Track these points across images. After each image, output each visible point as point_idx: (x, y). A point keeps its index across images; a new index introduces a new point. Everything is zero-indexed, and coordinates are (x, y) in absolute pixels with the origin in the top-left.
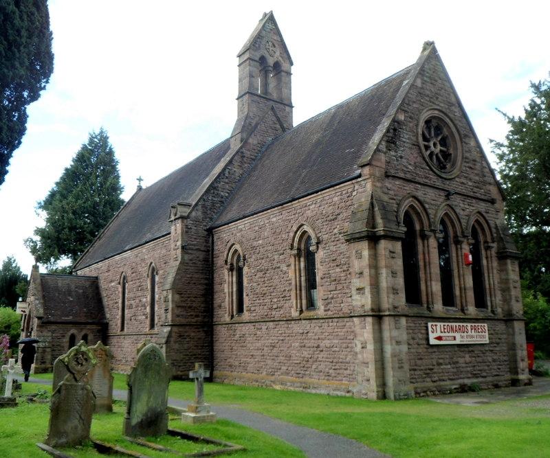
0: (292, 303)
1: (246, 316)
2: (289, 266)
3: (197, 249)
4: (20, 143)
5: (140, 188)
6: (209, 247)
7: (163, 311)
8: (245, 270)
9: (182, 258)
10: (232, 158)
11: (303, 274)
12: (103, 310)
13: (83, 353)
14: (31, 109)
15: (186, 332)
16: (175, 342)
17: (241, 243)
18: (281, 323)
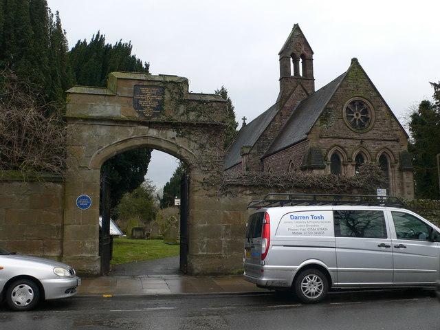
5: (244, 124)
10: (274, 118)
17: (273, 167)
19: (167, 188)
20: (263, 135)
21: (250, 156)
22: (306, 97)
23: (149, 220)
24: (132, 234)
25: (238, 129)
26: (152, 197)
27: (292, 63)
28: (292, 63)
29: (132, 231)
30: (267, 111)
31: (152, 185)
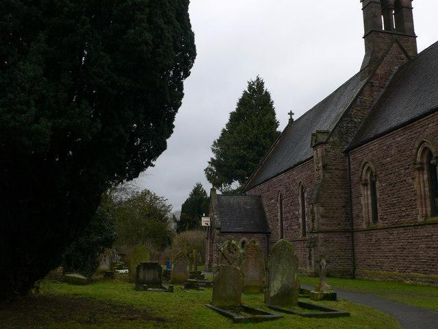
0: (418, 210)
1: (380, 223)
2: (413, 179)
3: (336, 169)
4: (181, 103)
5: (291, 120)
6: (346, 170)
7: (310, 221)
8: (378, 184)
9: (324, 177)
10: (362, 89)
11: (427, 185)
12: (267, 222)
13: (233, 245)
14: (186, 82)
15: (331, 238)
16: (322, 246)
17: (373, 161)
18: (409, 228)
19: (185, 207)
20: (346, 114)
21: (328, 146)
22: (405, 60)
23: (163, 246)
24: (138, 276)
25: (281, 129)
26: (167, 219)
27: (72, 275)
28: (72, 275)
29: (138, 268)
30: (330, 96)
31: (167, 204)
